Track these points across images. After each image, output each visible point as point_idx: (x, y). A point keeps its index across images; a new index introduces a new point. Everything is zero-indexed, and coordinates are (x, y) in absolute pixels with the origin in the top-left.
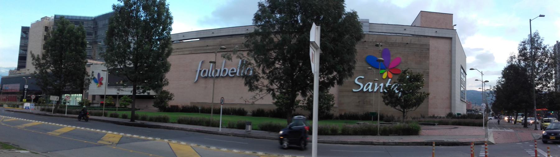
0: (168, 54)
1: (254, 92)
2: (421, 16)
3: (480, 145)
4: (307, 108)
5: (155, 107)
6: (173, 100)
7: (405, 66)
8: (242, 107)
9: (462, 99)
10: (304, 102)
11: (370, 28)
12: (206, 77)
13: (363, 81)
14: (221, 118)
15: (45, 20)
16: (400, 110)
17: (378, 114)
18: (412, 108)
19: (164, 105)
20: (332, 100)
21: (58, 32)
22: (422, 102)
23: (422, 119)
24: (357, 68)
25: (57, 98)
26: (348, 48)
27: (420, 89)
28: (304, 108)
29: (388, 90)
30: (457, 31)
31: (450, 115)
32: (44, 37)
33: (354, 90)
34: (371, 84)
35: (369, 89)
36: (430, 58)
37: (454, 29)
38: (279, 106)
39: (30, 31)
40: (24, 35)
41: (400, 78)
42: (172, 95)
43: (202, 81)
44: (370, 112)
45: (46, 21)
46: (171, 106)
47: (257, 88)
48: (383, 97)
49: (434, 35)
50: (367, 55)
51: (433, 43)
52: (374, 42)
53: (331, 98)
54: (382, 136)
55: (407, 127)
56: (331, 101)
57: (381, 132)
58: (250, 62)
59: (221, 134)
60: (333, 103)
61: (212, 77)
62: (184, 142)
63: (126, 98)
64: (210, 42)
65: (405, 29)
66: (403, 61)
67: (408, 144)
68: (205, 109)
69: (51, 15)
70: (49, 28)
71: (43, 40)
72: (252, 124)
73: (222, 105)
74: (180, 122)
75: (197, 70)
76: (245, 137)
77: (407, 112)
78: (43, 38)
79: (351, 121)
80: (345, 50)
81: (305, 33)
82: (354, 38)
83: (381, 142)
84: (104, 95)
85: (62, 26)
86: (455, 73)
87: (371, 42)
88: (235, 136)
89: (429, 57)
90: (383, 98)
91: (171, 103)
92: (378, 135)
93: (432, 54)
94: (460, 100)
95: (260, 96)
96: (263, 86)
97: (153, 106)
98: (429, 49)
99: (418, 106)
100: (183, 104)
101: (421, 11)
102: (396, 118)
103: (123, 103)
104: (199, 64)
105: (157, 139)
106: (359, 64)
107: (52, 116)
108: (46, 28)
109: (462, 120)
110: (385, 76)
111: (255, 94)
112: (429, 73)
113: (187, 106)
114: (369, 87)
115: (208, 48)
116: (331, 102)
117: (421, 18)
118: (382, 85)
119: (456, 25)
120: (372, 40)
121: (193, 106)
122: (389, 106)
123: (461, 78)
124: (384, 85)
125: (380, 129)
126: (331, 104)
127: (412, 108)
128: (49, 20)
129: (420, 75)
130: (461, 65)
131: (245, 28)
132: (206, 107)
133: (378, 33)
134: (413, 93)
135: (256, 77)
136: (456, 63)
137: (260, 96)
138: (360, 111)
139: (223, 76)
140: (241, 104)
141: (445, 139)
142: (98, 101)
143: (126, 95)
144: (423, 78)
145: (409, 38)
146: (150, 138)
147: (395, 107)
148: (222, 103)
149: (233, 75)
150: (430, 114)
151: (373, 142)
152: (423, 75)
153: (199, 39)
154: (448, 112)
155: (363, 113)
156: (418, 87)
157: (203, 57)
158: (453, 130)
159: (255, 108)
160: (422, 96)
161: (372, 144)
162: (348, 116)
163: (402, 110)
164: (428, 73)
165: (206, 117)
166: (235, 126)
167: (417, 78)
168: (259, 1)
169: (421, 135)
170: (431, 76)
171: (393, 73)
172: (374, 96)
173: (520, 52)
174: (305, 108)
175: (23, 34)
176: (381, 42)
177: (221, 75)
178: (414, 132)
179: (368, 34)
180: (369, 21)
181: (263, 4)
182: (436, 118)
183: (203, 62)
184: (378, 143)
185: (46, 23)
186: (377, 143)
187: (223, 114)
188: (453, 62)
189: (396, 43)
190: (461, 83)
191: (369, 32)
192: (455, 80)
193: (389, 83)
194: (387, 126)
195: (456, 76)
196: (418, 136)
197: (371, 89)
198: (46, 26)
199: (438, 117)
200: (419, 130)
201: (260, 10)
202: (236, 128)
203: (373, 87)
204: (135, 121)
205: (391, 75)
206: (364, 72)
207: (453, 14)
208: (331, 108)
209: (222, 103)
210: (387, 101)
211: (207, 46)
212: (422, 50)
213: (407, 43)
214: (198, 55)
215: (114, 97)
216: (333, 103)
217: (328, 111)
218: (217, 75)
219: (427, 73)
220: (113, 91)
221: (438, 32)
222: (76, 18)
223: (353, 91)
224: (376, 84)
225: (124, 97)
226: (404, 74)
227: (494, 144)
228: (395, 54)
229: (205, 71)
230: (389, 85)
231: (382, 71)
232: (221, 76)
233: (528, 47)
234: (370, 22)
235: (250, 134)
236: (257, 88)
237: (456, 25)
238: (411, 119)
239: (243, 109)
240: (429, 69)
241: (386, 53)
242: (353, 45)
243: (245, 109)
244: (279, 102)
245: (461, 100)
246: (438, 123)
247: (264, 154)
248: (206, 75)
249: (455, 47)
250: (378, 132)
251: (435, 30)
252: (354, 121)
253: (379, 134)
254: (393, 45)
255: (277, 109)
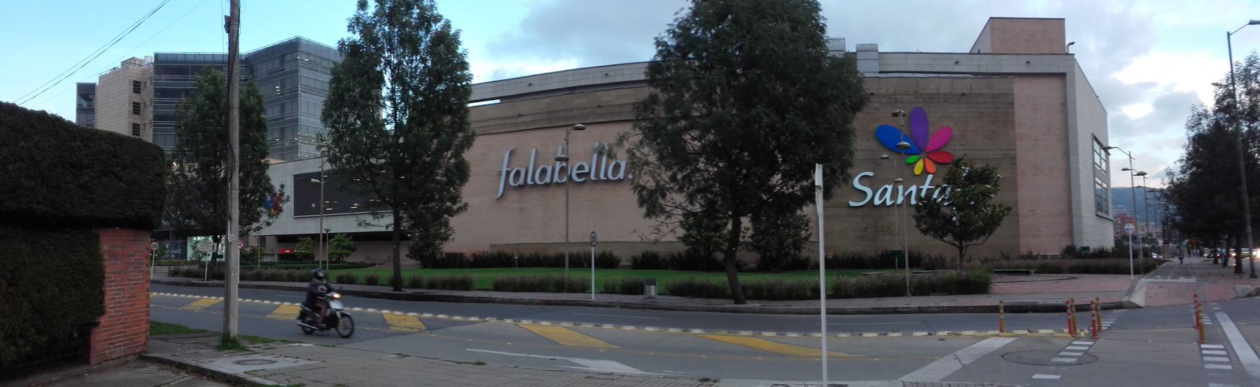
0: (468, 142)
1: (658, 219)
2: (992, 28)
3: (1110, 311)
4: (752, 246)
5: (411, 258)
6: (453, 240)
7: (962, 145)
8: (608, 250)
9: (1100, 214)
10: (745, 233)
11: (880, 64)
12: (521, 187)
13: (874, 183)
14: (593, 275)
15: (131, 67)
16: (954, 244)
17: (904, 252)
18: (977, 239)
19: (433, 253)
20: (806, 228)
21: (207, 102)
22: (999, 225)
23: (1005, 263)
24: (858, 156)
25: (213, 247)
26: (838, 130)
27: (991, 198)
28: (747, 247)
29: (925, 202)
30: (1075, 56)
31: (1070, 251)
32: (132, 105)
33: (852, 204)
34: (890, 188)
35: (885, 200)
36: (1016, 123)
37: (1070, 53)
38: (691, 245)
39: (98, 93)
40: (85, 104)
41: (948, 177)
42: (450, 230)
43: (513, 196)
44: (891, 251)
45: (135, 68)
46: (447, 254)
47: (663, 211)
48: (915, 217)
49: (1023, 69)
50: (877, 125)
51: (1021, 89)
52: (890, 95)
53: (802, 224)
54: (917, 297)
55: (964, 277)
56: (802, 229)
57: (913, 290)
58: (647, 160)
59: (597, 306)
60: (808, 233)
61: (535, 185)
62: (547, 321)
63: (342, 241)
64: (526, 106)
65: (957, 62)
66: (956, 132)
67: (966, 310)
68: (525, 257)
69: (146, 53)
70: (142, 86)
71: (132, 113)
72: (657, 283)
73: (593, 248)
74: (498, 287)
75: (501, 171)
76: (645, 308)
77: (967, 246)
78: (132, 109)
79: (850, 271)
80: (834, 134)
81: (758, 106)
82: (849, 109)
83: (913, 306)
84: (319, 234)
85: (214, 87)
86: (1076, 154)
87: (884, 96)
88: (625, 307)
89: (1013, 122)
90: (917, 220)
91: (448, 247)
92: (907, 296)
93: (1022, 114)
94: (1094, 215)
95: (668, 227)
96: (676, 207)
97: (408, 256)
98: (1012, 104)
99: (990, 234)
100: (474, 250)
101: (991, 18)
102: (948, 260)
103: (334, 251)
104: (503, 157)
105: (488, 319)
106: (862, 145)
107: (207, 285)
108: (137, 86)
109: (1104, 262)
110: (918, 169)
111: (659, 224)
112: (1015, 158)
113: (484, 253)
114: (884, 196)
115: (521, 120)
116: (803, 232)
117: (992, 34)
118: (913, 188)
119: (1072, 43)
120: (887, 91)
121: (498, 252)
122: (929, 238)
123: (1094, 163)
124: (919, 190)
125: (910, 283)
126: (802, 236)
127: (977, 239)
128: (140, 66)
129: (989, 169)
130: (1092, 134)
131: (602, 72)
132: (552, 253)
133: (897, 75)
134: (976, 209)
135: (661, 191)
136: (1079, 130)
137: (668, 227)
138: (868, 249)
139: (559, 181)
140: (604, 242)
141: (1040, 300)
142: (272, 250)
143: (342, 234)
144: (996, 174)
145: (966, 81)
146: (473, 319)
147: (941, 238)
148: (594, 243)
149: (583, 179)
150: (1024, 251)
151: (897, 308)
152: (996, 169)
153: (498, 101)
154: (1065, 243)
155: (876, 254)
156: (986, 195)
157: (511, 141)
158: (1062, 283)
159: (638, 252)
160: (995, 213)
161: (895, 311)
162: (842, 259)
163: (958, 244)
164: (1013, 160)
165: (555, 274)
166: (618, 289)
167: (983, 176)
168: (657, 36)
169: (993, 294)
170: (1021, 165)
171: (936, 163)
172: (896, 214)
173: (1218, 102)
174: (749, 247)
175: (82, 100)
176: (906, 93)
177: (556, 179)
178: (980, 287)
179: (877, 77)
180: (877, 49)
181: (665, 43)
182: (1036, 258)
183: (512, 153)
184: (907, 309)
185: (135, 73)
186: (904, 310)
187: (596, 266)
188: (1071, 129)
189: (940, 94)
190: (1095, 176)
191: (880, 72)
192: (1078, 170)
193: (930, 185)
194: (924, 275)
195: (1081, 160)
196: (986, 295)
197: (891, 200)
198: (135, 79)
199: (1039, 257)
200: (990, 283)
201: (660, 52)
202: (618, 293)
203: (894, 195)
204: (403, 289)
205: (932, 167)
206: (874, 163)
207: (1064, 19)
208: (804, 245)
209: (594, 243)
210: (924, 226)
211: (520, 115)
212: (997, 108)
213: (963, 94)
214: (501, 137)
215: (315, 237)
216: (808, 233)
217: (797, 252)
218: (547, 180)
219: (1012, 159)
220: (309, 226)
221: (1032, 61)
222: (195, 57)
223: (848, 204)
224: (901, 188)
225: (337, 237)
226: (956, 167)
227: (1140, 307)
228: (938, 119)
229: (518, 174)
230: (928, 189)
231: (911, 159)
232: (555, 182)
233: (1240, 89)
234: (880, 51)
235: (655, 302)
236: (663, 211)
237: (1072, 43)
238: (979, 263)
239: (611, 255)
240: (1015, 150)
241: (918, 118)
242: (847, 121)
243: (616, 254)
244: (690, 236)
245: (1097, 215)
246: (1035, 270)
247: (704, 332)
248: (521, 181)
249: (1074, 95)
250: (908, 290)
251: (1024, 59)
252: (858, 271)
253: (909, 294)
254: (932, 98)
255: (688, 252)
